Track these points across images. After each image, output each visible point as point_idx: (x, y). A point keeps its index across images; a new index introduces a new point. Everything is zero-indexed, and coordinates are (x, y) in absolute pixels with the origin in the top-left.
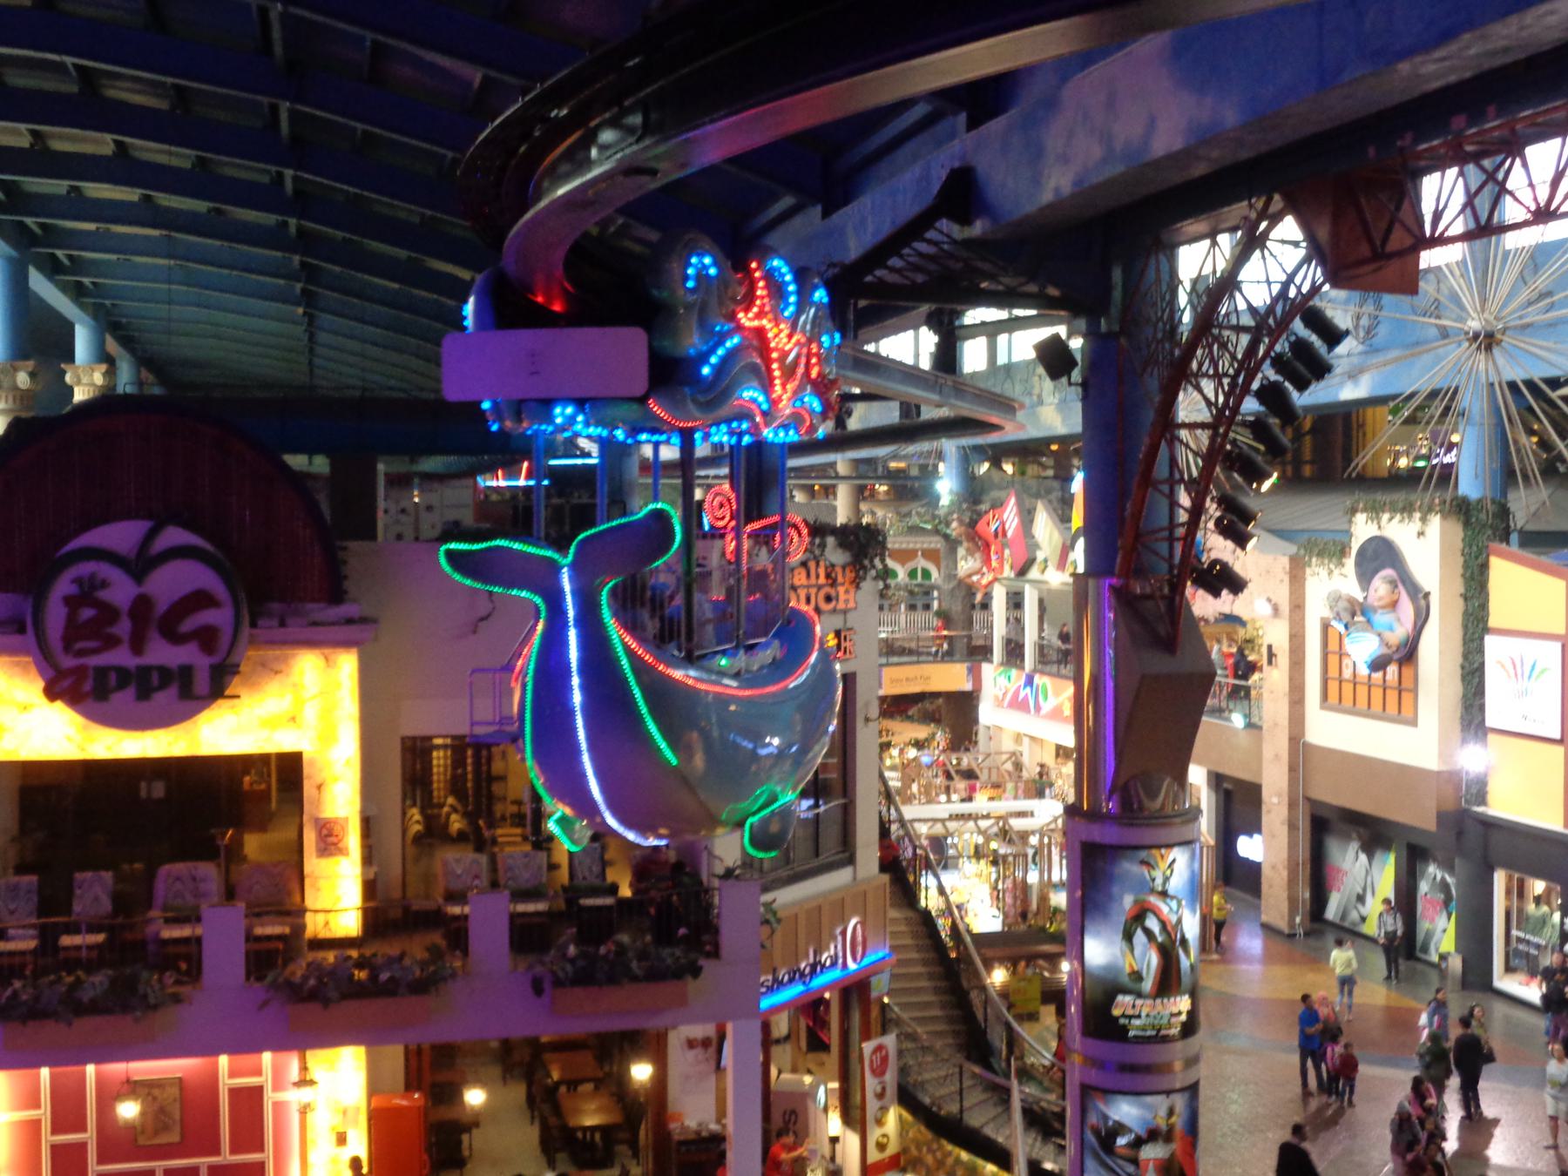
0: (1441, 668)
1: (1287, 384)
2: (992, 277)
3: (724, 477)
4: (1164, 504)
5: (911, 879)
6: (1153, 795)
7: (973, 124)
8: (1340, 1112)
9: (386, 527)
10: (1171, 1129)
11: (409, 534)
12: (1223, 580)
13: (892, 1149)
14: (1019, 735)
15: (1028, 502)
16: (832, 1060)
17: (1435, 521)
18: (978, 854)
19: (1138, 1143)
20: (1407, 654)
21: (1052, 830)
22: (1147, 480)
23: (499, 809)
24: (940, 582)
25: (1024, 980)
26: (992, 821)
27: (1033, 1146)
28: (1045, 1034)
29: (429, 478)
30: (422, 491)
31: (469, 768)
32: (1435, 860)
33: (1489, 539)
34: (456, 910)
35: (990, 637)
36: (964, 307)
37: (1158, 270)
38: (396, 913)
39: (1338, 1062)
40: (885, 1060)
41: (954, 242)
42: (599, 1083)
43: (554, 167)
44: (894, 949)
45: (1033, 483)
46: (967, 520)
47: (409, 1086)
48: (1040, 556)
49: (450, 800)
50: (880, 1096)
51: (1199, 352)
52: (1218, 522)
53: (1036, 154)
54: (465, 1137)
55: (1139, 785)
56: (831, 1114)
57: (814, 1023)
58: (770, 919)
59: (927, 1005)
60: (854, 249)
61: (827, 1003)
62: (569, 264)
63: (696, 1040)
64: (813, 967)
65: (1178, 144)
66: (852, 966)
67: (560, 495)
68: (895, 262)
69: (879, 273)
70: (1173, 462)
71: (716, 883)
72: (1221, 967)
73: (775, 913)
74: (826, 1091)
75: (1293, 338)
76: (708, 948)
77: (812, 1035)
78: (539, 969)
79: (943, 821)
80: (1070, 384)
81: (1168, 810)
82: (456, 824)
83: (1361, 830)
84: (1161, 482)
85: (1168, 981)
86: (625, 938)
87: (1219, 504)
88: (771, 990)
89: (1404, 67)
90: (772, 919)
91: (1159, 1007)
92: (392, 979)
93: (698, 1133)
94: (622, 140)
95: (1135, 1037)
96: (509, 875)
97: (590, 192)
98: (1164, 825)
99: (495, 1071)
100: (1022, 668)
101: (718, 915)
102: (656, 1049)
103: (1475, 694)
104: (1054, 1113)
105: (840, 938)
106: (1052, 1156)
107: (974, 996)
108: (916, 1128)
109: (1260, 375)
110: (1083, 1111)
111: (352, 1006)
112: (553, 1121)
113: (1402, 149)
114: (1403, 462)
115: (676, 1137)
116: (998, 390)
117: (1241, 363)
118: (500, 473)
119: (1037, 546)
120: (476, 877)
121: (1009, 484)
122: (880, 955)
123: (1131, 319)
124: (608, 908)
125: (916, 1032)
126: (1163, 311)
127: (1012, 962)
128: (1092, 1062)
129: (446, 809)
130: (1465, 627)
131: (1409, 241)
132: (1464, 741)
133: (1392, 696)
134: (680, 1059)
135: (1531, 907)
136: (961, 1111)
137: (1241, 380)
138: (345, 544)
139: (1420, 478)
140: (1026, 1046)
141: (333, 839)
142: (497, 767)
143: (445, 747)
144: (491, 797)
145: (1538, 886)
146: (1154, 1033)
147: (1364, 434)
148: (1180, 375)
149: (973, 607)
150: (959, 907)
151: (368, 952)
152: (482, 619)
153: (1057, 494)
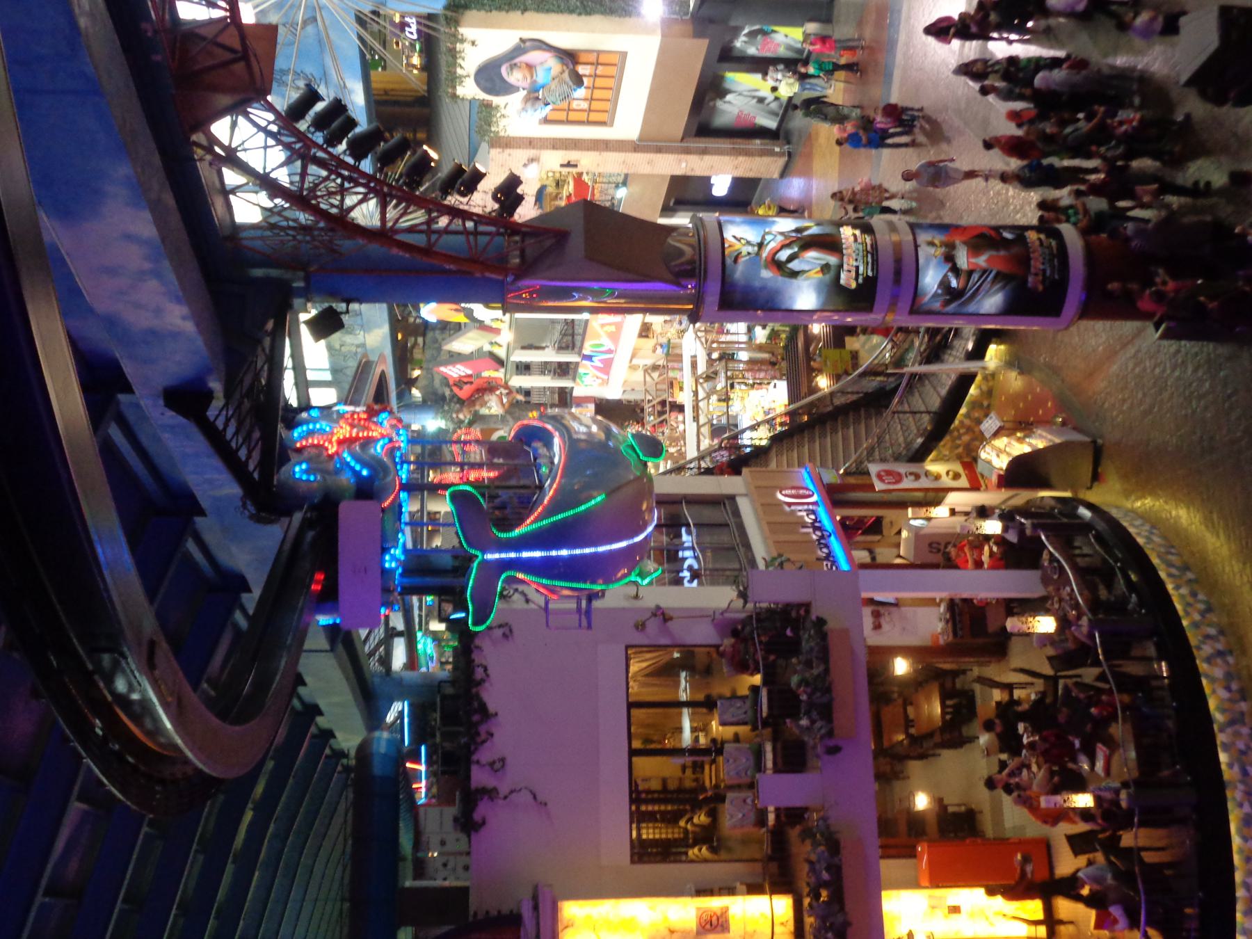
1: (350, 136)
2: (257, 376)
3: (420, 601)
4: (446, 238)
5: (748, 450)
6: (681, 253)
7: (128, 389)
8: (928, 119)
9: (457, 879)
10: (943, 244)
11: (463, 860)
12: (509, 193)
13: (958, 468)
14: (630, 367)
15: (444, 357)
16: (889, 514)
17: (464, 31)
18: (726, 399)
19: (955, 270)
20: (570, 57)
21: (707, 341)
22: (427, 251)
23: (689, 784)
24: (507, 429)
25: (825, 361)
26: (700, 388)
27: (956, 357)
28: (867, 347)
29: (418, 844)
30: (428, 850)
31: (656, 808)
32: (731, 41)
34: (771, 818)
35: (552, 390)
36: (282, 404)
37: (253, 239)
38: (773, 867)
39: (889, 120)
40: (889, 473)
41: (226, 406)
42: (907, 702)
43: (161, 745)
44: (801, 464)
45: (429, 353)
46: (458, 406)
47: (911, 854)
48: (487, 348)
49: (682, 823)
50: (917, 477)
51: (323, 206)
52: (463, 195)
53: (154, 335)
54: (951, 809)
55: (673, 264)
56: (933, 515)
57: (860, 529)
58: (778, 562)
59: (845, 439)
60: (233, 490)
61: (844, 519)
62: (237, 721)
63: (874, 623)
64: (815, 529)
65: (147, 215)
66: (815, 498)
67: (434, 736)
68: (243, 454)
69: (251, 467)
70: (411, 230)
71: (750, 606)
72: (814, 208)
73: (774, 559)
74: (915, 520)
75: (312, 129)
76: (802, 612)
77: (868, 531)
78: (820, 749)
79: (699, 428)
80: (347, 312)
81: (694, 241)
82: (701, 818)
83: (707, 98)
84: (429, 239)
85: (829, 243)
86: (795, 680)
87: (450, 194)
88: (834, 562)
89: (83, 22)
90: (779, 560)
92: (828, 869)
93: (947, 622)
94: (124, 672)
95: (872, 270)
96: (743, 774)
97: (170, 699)
98: (706, 243)
99: (898, 785)
100: (577, 364)
101: (776, 603)
102: (881, 655)
104: (930, 340)
105: (793, 508)
106: (963, 342)
107: (839, 401)
108: (941, 449)
109: (342, 157)
110: (930, 313)
111: (849, 905)
112: (937, 739)
113: (156, 32)
114: (416, 60)
115: (951, 638)
116: (350, 379)
117: (331, 172)
118: (414, 786)
119: (480, 350)
120: (745, 801)
121: (429, 373)
122: (806, 476)
123: (295, 262)
124: (770, 693)
125: (866, 448)
126: (288, 235)
127: (812, 372)
128: (893, 305)
129: (689, 827)
130: (548, 11)
131: (233, 30)
132: (639, 15)
133: (600, 70)
134: (890, 635)
136: (928, 412)
137: (346, 173)
138: (472, 913)
139: (429, 35)
140: (876, 362)
141: (714, 919)
142: (655, 785)
143: (639, 830)
144: (680, 790)
146: (869, 256)
147: (392, 90)
148: (341, 222)
149: (528, 403)
150: (766, 413)
151: (806, 890)
152: (535, 797)
153: (438, 334)
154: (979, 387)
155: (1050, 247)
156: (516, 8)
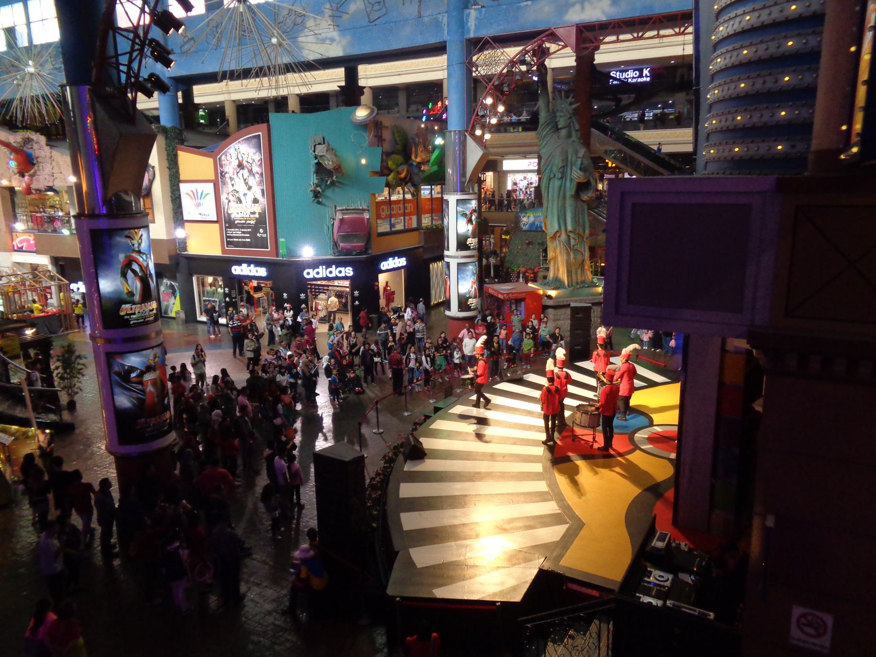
0: (163, 197)
4: (115, 72)
19: (142, 373)
32: (166, 277)
33: (176, 143)
85: (147, 295)
91: (144, 308)
95: (134, 323)
103: (178, 208)
130: (171, 180)
132: (175, 228)
135: (208, 288)
145: (210, 279)
146: (142, 320)
154: (17, 431)
155: (164, 426)
156: (170, 165)
